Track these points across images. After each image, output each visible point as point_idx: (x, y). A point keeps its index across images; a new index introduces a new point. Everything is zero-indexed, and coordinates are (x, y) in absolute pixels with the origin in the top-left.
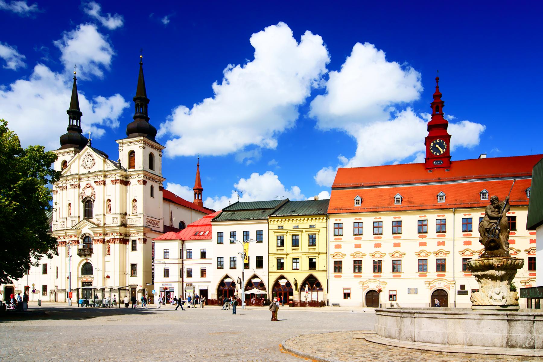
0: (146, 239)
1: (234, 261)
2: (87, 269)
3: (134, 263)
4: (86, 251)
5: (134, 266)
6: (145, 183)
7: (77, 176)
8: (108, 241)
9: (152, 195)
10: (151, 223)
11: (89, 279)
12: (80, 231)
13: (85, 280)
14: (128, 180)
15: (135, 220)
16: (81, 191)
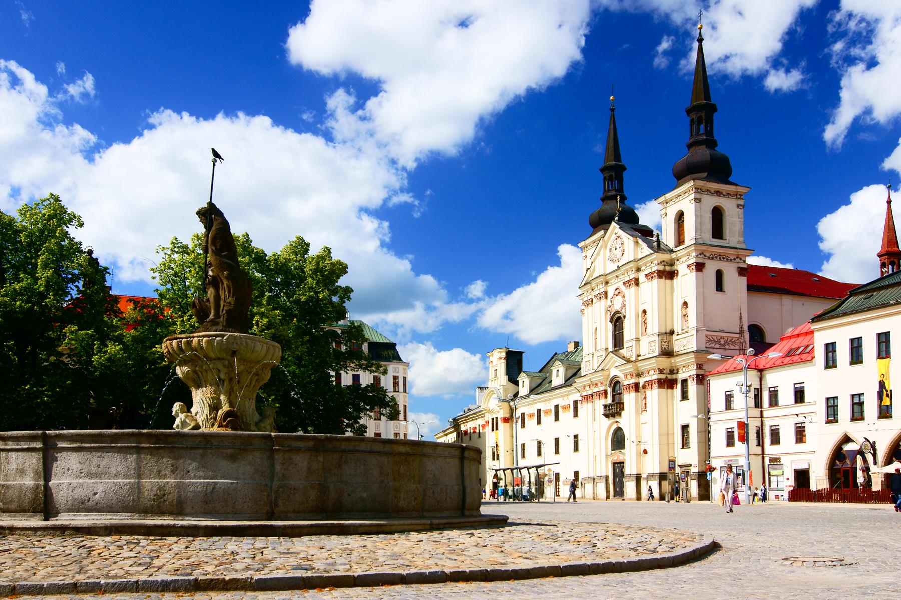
1: (861, 404)
2: (618, 441)
3: (685, 423)
4: (614, 410)
5: (685, 428)
6: (699, 267)
7: (601, 279)
8: (644, 387)
9: (719, 287)
10: (718, 342)
11: (621, 459)
12: (606, 373)
13: (615, 459)
14: (675, 268)
15: (685, 342)
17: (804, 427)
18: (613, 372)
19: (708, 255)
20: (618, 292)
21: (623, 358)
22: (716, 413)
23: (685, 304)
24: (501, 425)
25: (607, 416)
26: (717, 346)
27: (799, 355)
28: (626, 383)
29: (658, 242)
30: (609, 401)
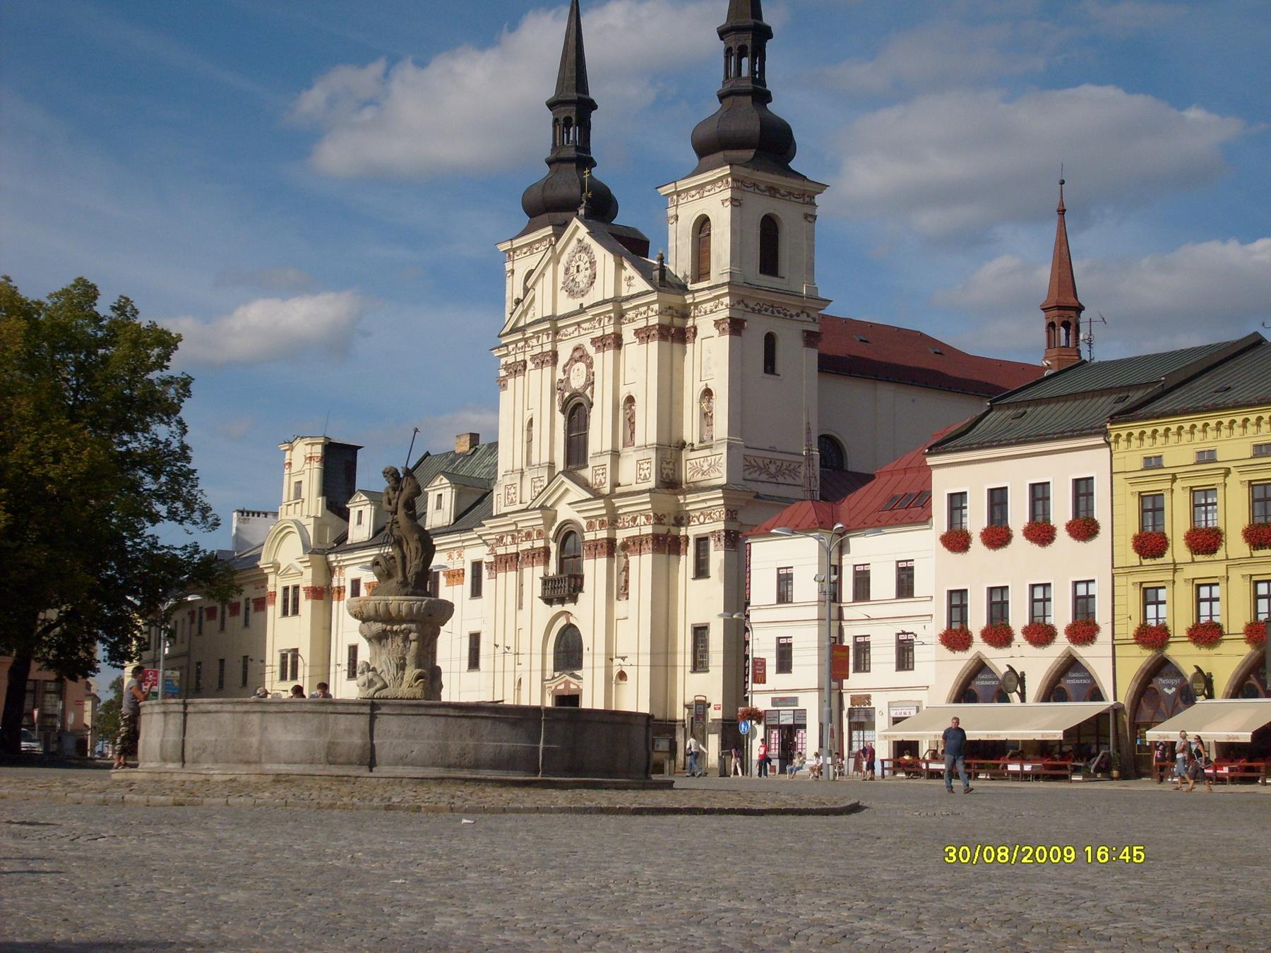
2: (568, 651)
4: (564, 587)
5: (700, 632)
8: (625, 546)
9: (770, 365)
10: (763, 469)
16: (560, 375)
18: (564, 512)
19: (751, 305)
20: (580, 355)
21: (585, 485)
22: (759, 608)
23: (708, 393)
24: (305, 605)
25: (549, 601)
26: (764, 477)
27: (909, 507)
28: (589, 536)
29: (663, 270)
30: (553, 569)
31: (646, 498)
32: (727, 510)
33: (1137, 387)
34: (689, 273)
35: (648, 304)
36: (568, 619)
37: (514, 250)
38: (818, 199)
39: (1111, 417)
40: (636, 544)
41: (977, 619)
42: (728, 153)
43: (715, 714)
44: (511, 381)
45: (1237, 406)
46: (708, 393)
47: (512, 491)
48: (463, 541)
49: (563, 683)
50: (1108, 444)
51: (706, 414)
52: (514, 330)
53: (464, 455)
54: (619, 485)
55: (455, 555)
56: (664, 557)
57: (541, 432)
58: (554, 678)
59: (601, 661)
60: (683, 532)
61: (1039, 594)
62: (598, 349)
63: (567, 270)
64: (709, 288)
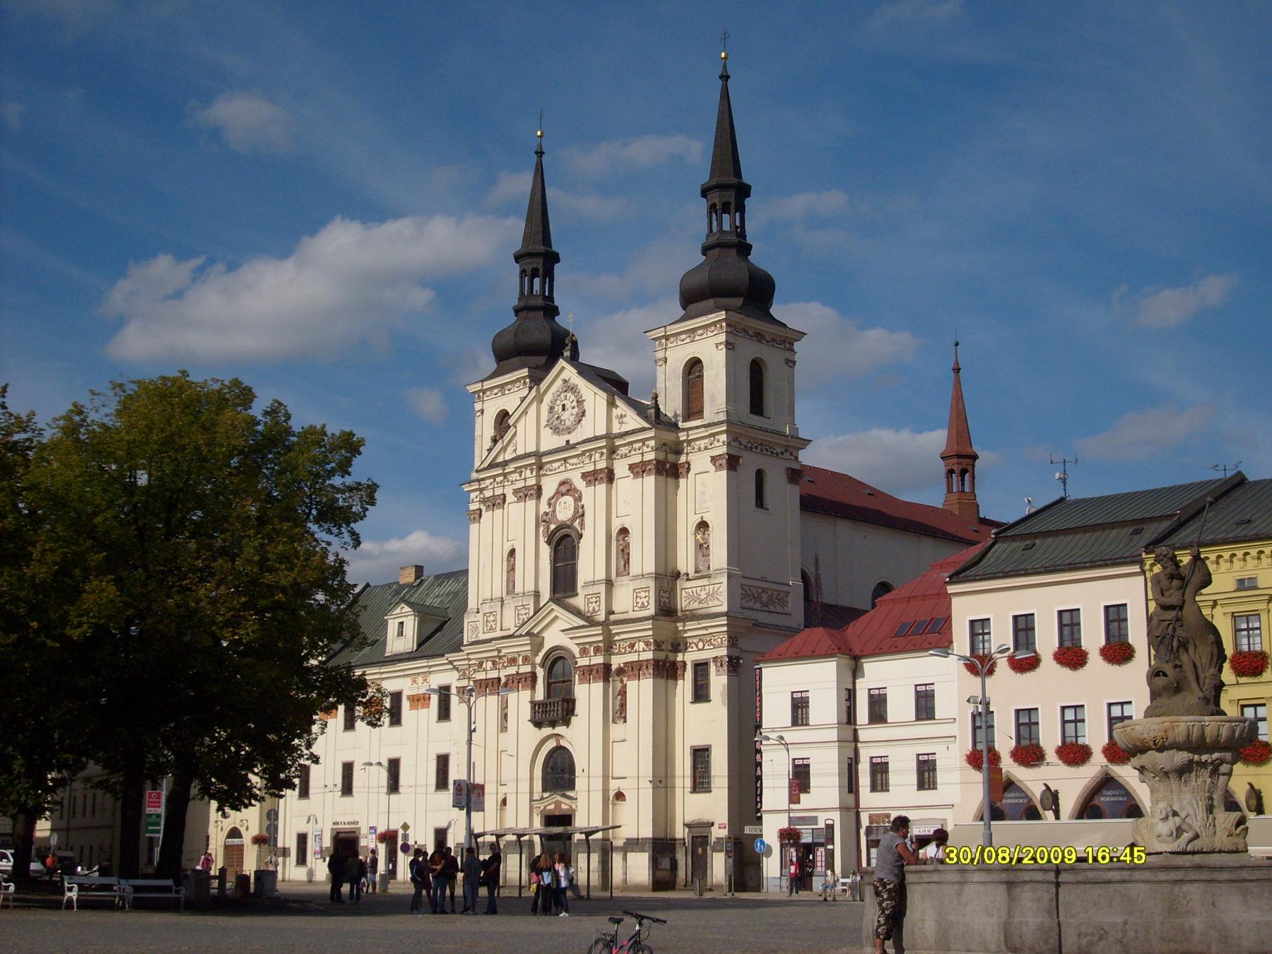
0: (738, 659)
2: (559, 772)
4: (555, 710)
5: (701, 755)
8: (620, 671)
9: (760, 501)
10: (758, 599)
16: (544, 507)
17: (808, 766)
18: (553, 638)
19: (744, 442)
20: (567, 488)
21: (577, 612)
23: (703, 525)
25: (538, 724)
26: (758, 606)
27: (929, 633)
28: (583, 662)
30: (540, 694)
31: (649, 624)
32: (729, 637)
33: (1152, 520)
34: (680, 412)
35: (643, 441)
36: (558, 742)
37: (484, 392)
38: (797, 346)
39: (1146, 547)
40: (634, 669)
41: (1005, 742)
42: (718, 300)
43: (719, 833)
44: (487, 515)
45: (1225, 542)
46: (703, 525)
47: (492, 618)
48: (430, 667)
49: (553, 803)
50: (1143, 572)
51: (701, 545)
52: (492, 466)
53: (410, 586)
54: (613, 613)
55: (420, 680)
56: (663, 681)
57: (525, 563)
58: (542, 798)
59: (597, 784)
60: (680, 657)
61: (1070, 715)
62: (589, 483)
63: (552, 408)
64: (704, 426)
